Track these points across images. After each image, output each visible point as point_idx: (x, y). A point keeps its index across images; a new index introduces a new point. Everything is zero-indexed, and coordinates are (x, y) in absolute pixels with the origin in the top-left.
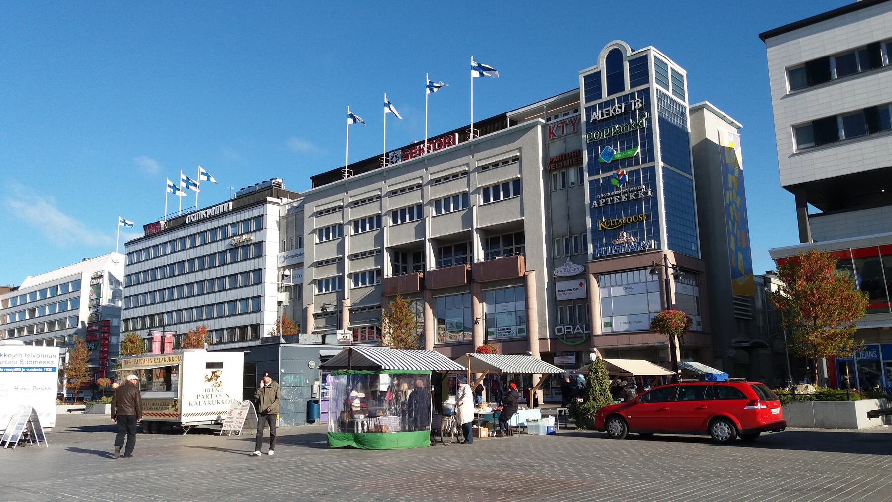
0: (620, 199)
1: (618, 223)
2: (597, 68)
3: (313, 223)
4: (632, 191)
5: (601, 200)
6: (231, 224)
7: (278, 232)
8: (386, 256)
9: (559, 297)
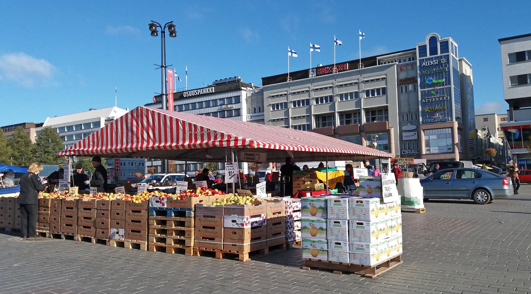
0: (436, 99)
1: (434, 109)
3: (268, 102)
4: (441, 97)
5: (427, 100)
6: (219, 99)
8: (313, 118)
9: (404, 139)
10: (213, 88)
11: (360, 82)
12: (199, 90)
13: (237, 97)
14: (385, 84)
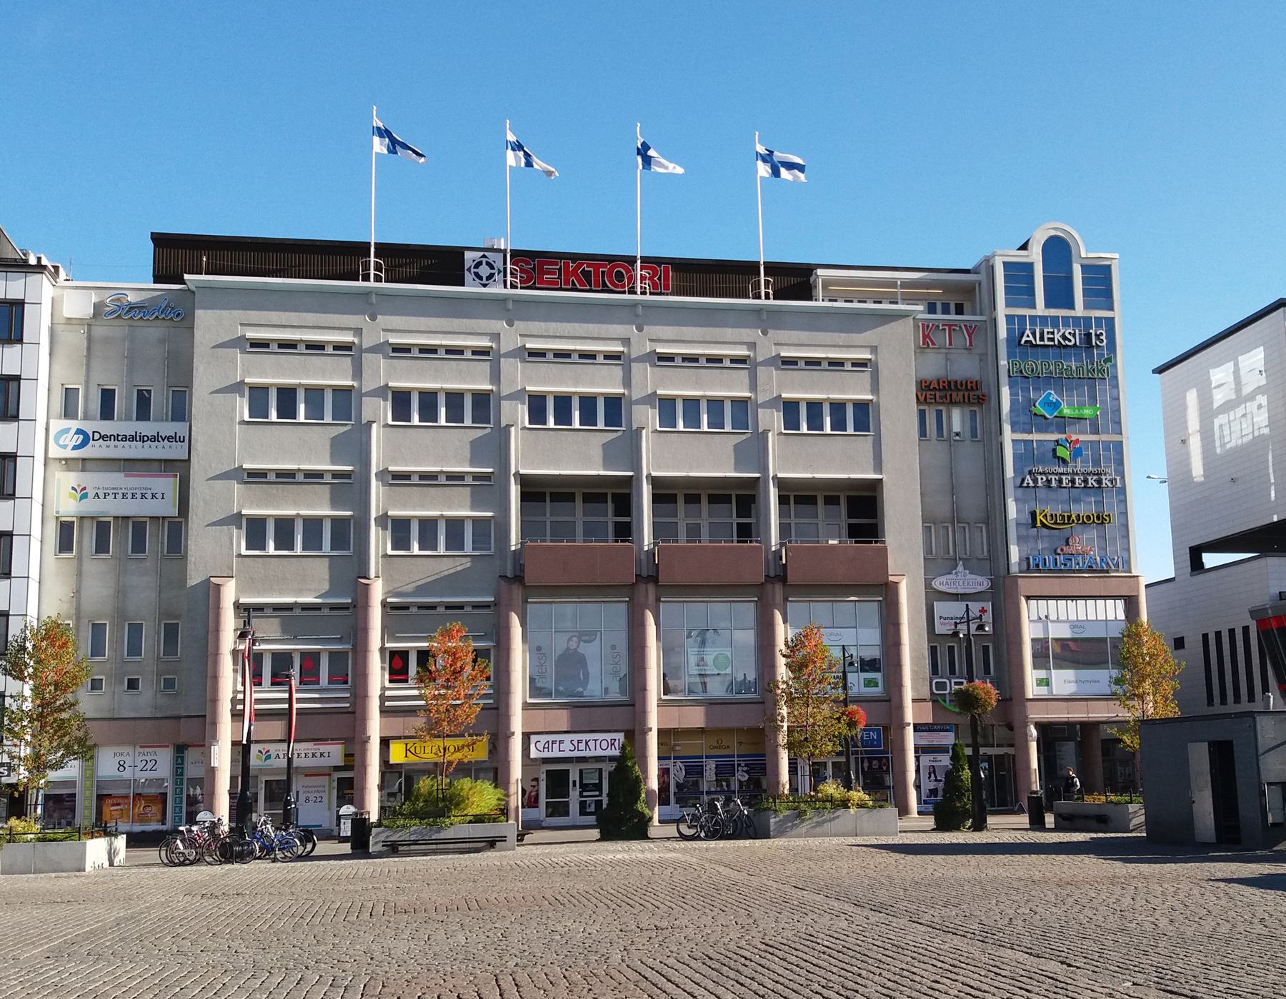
2: (1028, 256)
5: (1039, 477)
7: (48, 356)
11: (760, 359)
14: (868, 387)
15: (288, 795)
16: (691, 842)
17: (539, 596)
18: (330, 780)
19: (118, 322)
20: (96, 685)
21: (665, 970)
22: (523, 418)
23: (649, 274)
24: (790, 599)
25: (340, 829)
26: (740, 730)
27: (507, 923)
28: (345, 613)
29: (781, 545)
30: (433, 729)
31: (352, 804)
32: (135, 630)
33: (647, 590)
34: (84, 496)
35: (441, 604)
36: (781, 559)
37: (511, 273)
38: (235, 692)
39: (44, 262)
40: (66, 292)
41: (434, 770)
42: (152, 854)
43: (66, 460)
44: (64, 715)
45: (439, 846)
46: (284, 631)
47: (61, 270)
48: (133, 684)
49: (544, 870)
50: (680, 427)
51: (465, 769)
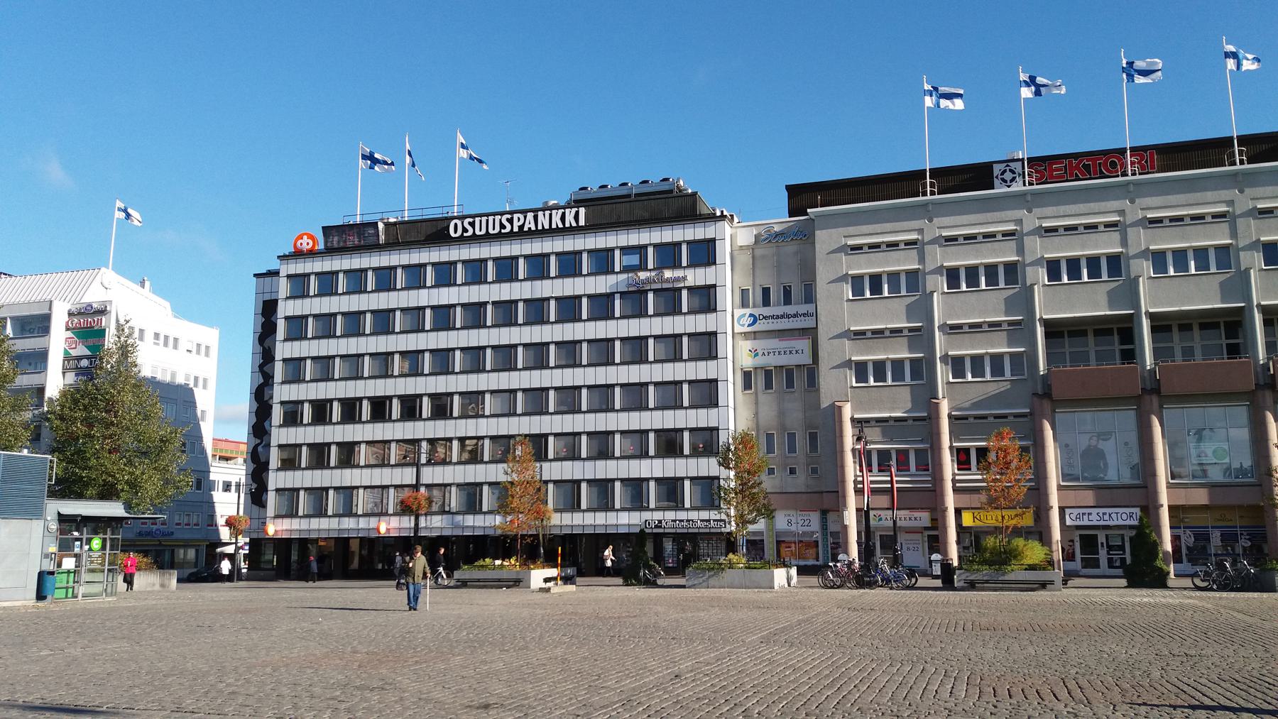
10: (582, 211)
12: (521, 216)
13: (539, 258)
15: (896, 545)
16: (1205, 592)
17: (1065, 407)
18: (922, 536)
19: (770, 244)
20: (771, 471)
21: (1200, 687)
22: (1043, 278)
23: (1137, 159)
24: (1165, 406)
25: (932, 570)
26: (1240, 507)
27: (1064, 643)
28: (924, 423)
29: (1269, 359)
30: (993, 503)
31: (939, 553)
32: (792, 437)
33: (1151, 400)
34: (756, 355)
35: (991, 415)
36: (1269, 370)
37: (1028, 175)
38: (856, 476)
39: (725, 213)
40: (738, 230)
41: (996, 530)
42: (814, 580)
43: (745, 333)
44: (754, 491)
45: (1004, 585)
46: (884, 436)
47: (735, 216)
48: (792, 471)
49: (1087, 607)
50: (1172, 272)
51: (1017, 532)
